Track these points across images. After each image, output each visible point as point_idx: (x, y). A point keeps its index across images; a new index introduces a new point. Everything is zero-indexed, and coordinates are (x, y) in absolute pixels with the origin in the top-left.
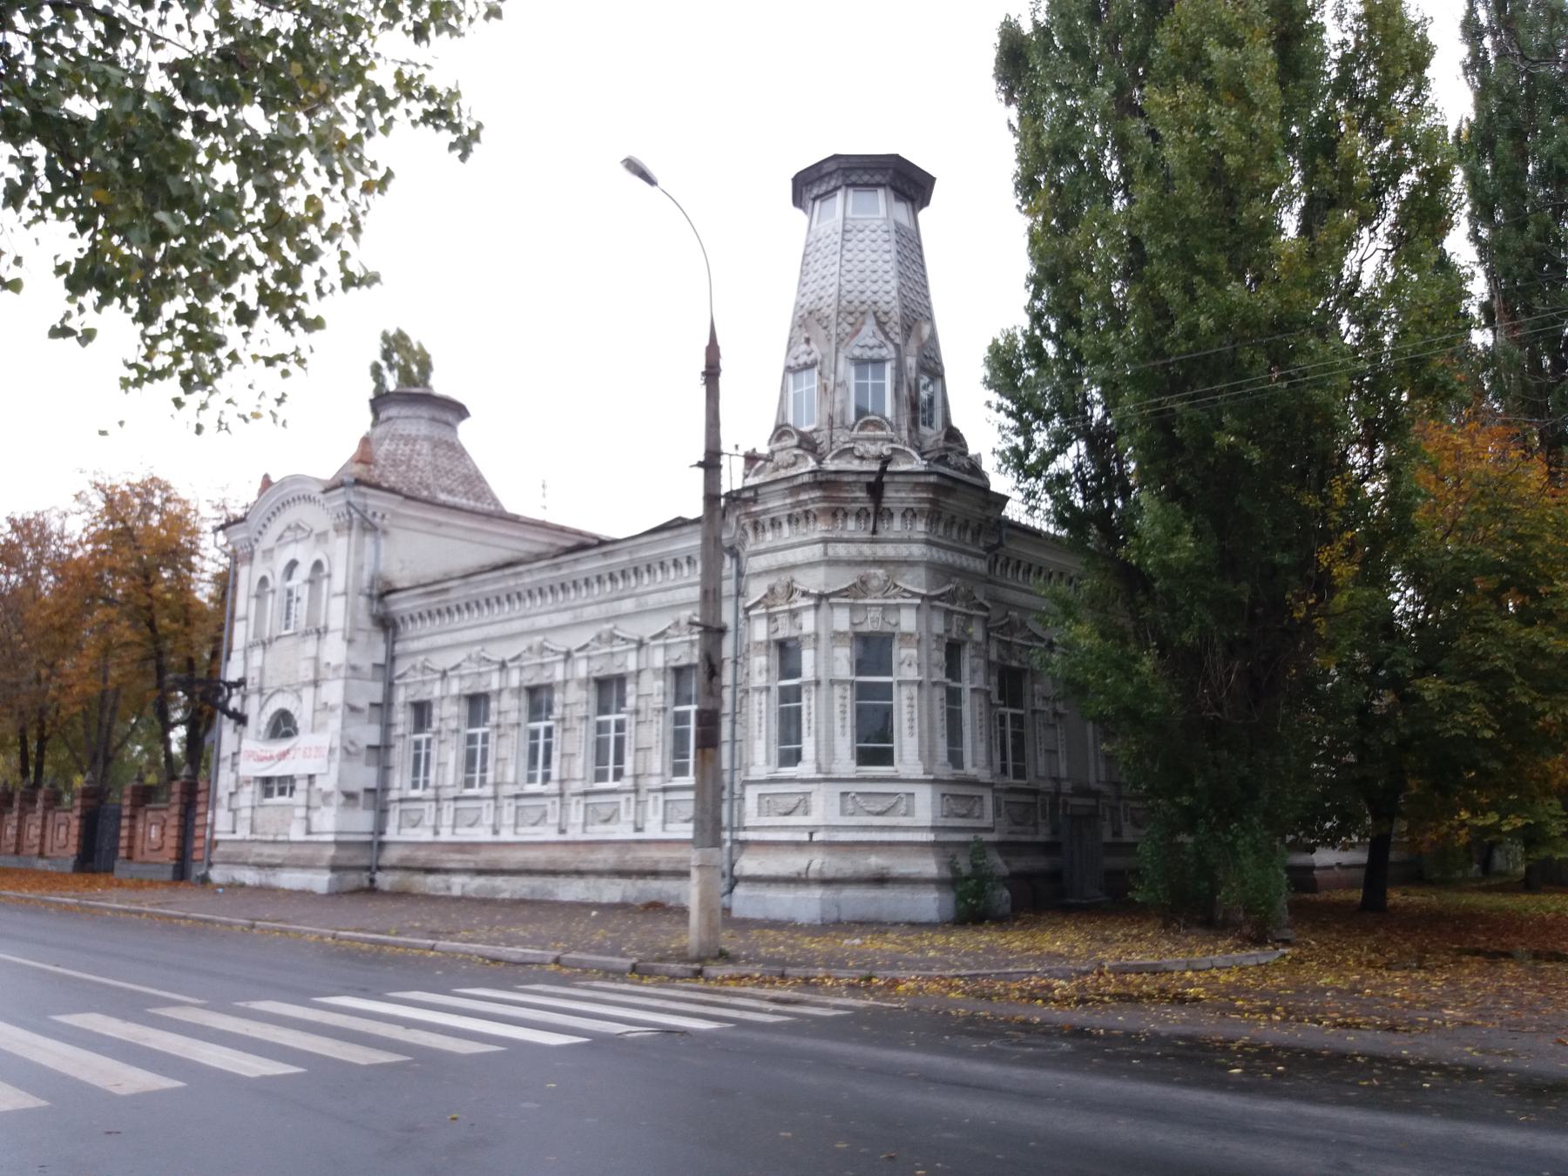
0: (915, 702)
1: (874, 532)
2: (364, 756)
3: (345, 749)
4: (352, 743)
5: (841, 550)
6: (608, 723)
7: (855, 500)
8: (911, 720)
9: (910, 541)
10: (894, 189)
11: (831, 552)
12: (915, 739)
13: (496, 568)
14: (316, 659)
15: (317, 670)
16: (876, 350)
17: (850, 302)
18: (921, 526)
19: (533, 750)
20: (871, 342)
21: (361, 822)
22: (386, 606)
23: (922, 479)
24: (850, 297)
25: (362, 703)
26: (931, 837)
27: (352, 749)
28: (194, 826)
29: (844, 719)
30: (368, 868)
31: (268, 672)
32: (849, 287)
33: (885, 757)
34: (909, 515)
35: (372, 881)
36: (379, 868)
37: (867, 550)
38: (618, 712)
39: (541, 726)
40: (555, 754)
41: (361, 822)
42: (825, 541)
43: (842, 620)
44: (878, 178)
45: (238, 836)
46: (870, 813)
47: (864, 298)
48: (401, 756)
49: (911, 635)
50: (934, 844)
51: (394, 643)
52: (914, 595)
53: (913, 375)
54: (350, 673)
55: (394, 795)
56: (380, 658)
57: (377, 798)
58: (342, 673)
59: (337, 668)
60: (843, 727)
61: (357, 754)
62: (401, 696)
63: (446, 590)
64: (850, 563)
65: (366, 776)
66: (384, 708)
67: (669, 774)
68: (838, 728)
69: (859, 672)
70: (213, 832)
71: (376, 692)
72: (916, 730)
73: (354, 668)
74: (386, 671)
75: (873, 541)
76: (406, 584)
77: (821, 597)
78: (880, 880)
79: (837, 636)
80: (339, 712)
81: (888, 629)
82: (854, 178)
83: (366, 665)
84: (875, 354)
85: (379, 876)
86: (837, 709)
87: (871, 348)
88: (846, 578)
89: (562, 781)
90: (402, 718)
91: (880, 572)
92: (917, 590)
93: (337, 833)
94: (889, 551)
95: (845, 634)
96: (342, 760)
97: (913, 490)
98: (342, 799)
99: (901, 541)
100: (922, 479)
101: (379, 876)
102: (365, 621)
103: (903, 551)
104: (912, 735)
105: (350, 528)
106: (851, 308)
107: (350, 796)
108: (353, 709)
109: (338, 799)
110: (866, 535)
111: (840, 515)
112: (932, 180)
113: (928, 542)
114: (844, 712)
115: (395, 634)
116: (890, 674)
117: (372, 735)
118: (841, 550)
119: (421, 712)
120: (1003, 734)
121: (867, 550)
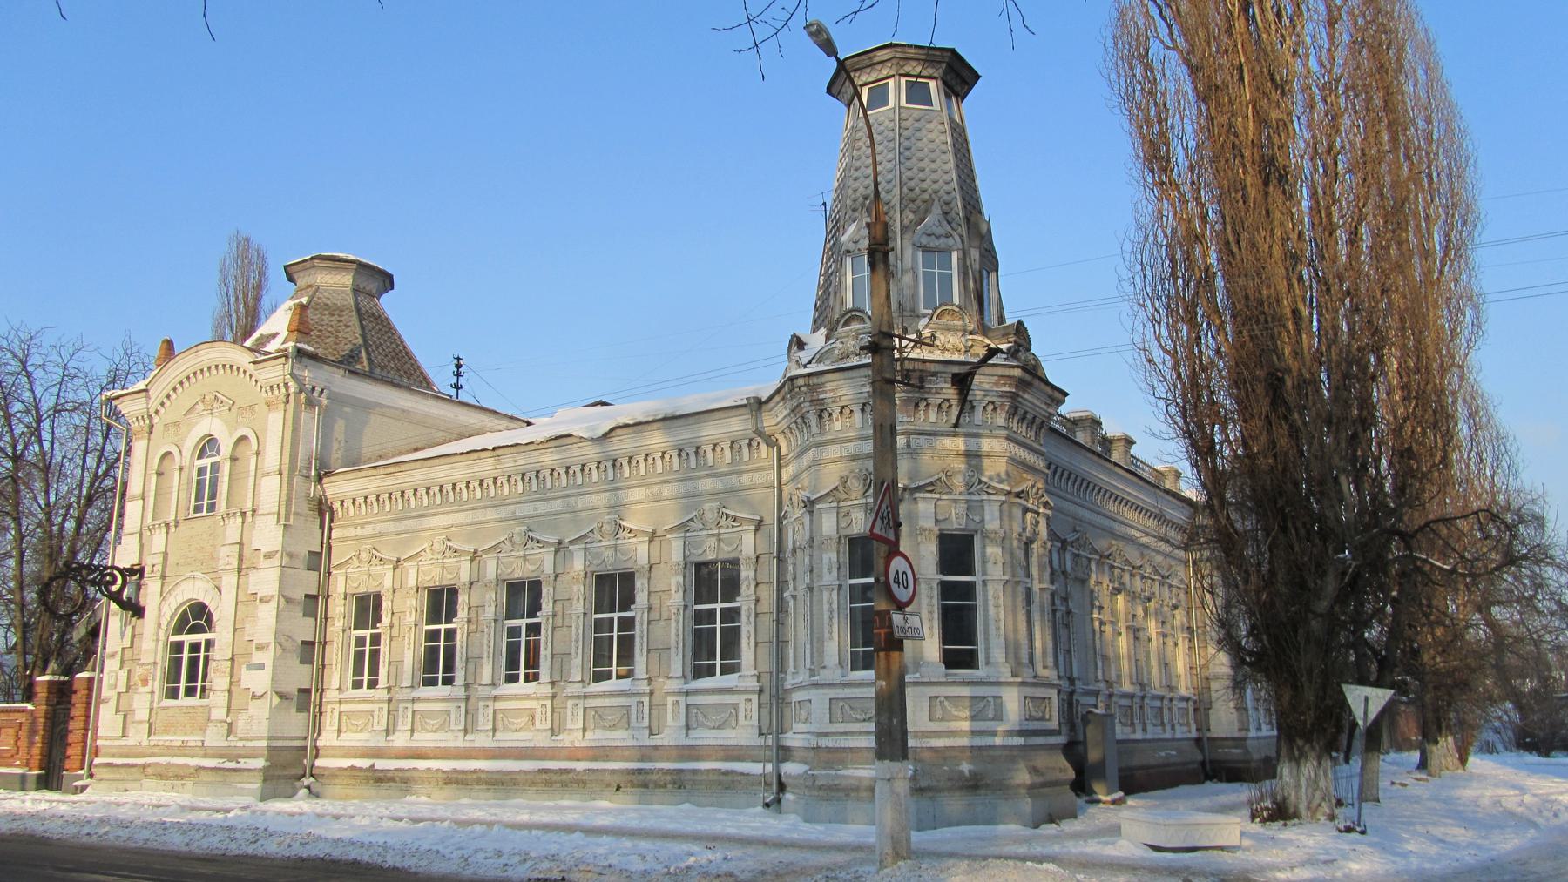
6: (439, 631)
10: (945, 83)
13: (557, 438)
14: (241, 544)
15: (241, 558)
16: (942, 240)
17: (911, 190)
19: (359, 656)
20: (939, 231)
23: (1007, 372)
24: (911, 184)
31: (171, 559)
32: (909, 174)
33: (536, 677)
38: (374, 627)
39: (367, 633)
40: (545, 653)
44: (931, 71)
45: (130, 741)
46: (857, 720)
47: (924, 185)
48: (338, 654)
53: (977, 266)
54: (286, 560)
58: (277, 561)
59: (269, 556)
62: (339, 585)
66: (313, 604)
67: (690, 675)
69: (943, 571)
74: (318, 561)
76: (656, 425)
80: (274, 604)
81: (972, 526)
82: (907, 69)
84: (942, 242)
87: (938, 237)
89: (389, 689)
90: (340, 610)
97: (996, 384)
98: (276, 700)
100: (1007, 372)
106: (912, 195)
108: (288, 600)
111: (922, 407)
112: (977, 77)
116: (970, 572)
119: (368, 608)
120: (204, 680)
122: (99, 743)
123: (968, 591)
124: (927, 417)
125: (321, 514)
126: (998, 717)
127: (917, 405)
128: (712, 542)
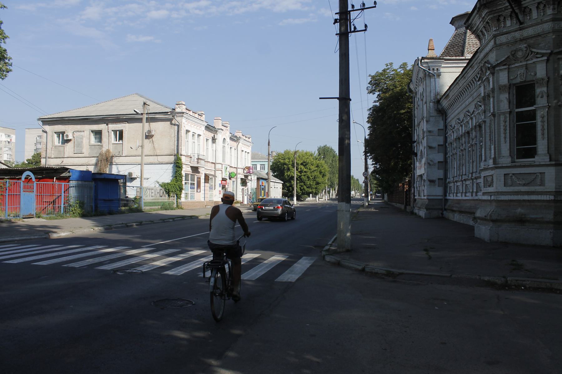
0: (546, 119)
1: (521, 23)
2: (437, 165)
3: (429, 163)
4: (431, 161)
5: (503, 39)
7: (506, 9)
8: (543, 130)
9: (542, 22)
11: (498, 42)
12: (545, 141)
18: (549, 11)
21: (438, 191)
22: (442, 105)
25: (435, 145)
26: (552, 198)
27: (431, 163)
28: (547, 195)
29: (505, 134)
30: (442, 209)
33: (532, 153)
34: (542, 6)
35: (442, 214)
36: (445, 210)
37: (517, 35)
41: (438, 191)
42: (495, 37)
43: (503, 78)
46: (520, 185)
49: (543, 79)
50: (554, 201)
51: (446, 120)
52: (543, 55)
55: (448, 180)
56: (441, 126)
57: (444, 182)
60: (505, 138)
61: (434, 165)
63: (448, 95)
64: (507, 44)
65: (440, 174)
68: (502, 135)
70: (414, 196)
71: (441, 140)
72: (546, 136)
73: (430, 132)
75: (521, 29)
77: (494, 67)
78: (521, 221)
79: (502, 88)
83: (435, 129)
85: (445, 212)
86: (502, 128)
88: (505, 54)
91: (523, 46)
92: (544, 51)
93: (428, 196)
94: (529, 32)
95: (505, 86)
96: (428, 168)
98: (429, 183)
99: (537, 24)
101: (445, 212)
102: (434, 113)
103: (539, 29)
104: (543, 139)
105: (425, 77)
107: (432, 181)
108: (430, 147)
109: (427, 183)
110: (517, 26)
111: (502, 19)
113: (554, 20)
114: (505, 130)
115: (446, 116)
117: (440, 157)
118: (503, 39)
121: (517, 35)
122: (416, 198)
123: (532, 115)
124: (505, 24)
125: (442, 114)
126: (542, 184)
127: (498, 20)
128: (522, 71)
